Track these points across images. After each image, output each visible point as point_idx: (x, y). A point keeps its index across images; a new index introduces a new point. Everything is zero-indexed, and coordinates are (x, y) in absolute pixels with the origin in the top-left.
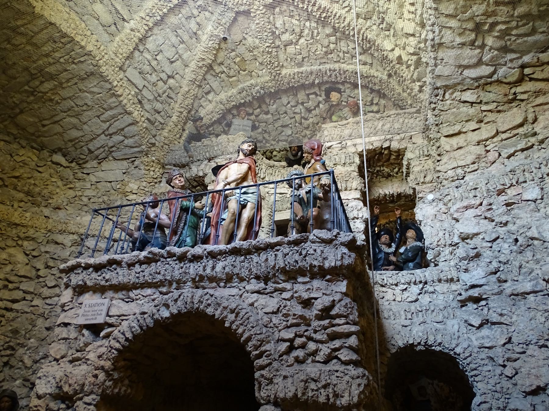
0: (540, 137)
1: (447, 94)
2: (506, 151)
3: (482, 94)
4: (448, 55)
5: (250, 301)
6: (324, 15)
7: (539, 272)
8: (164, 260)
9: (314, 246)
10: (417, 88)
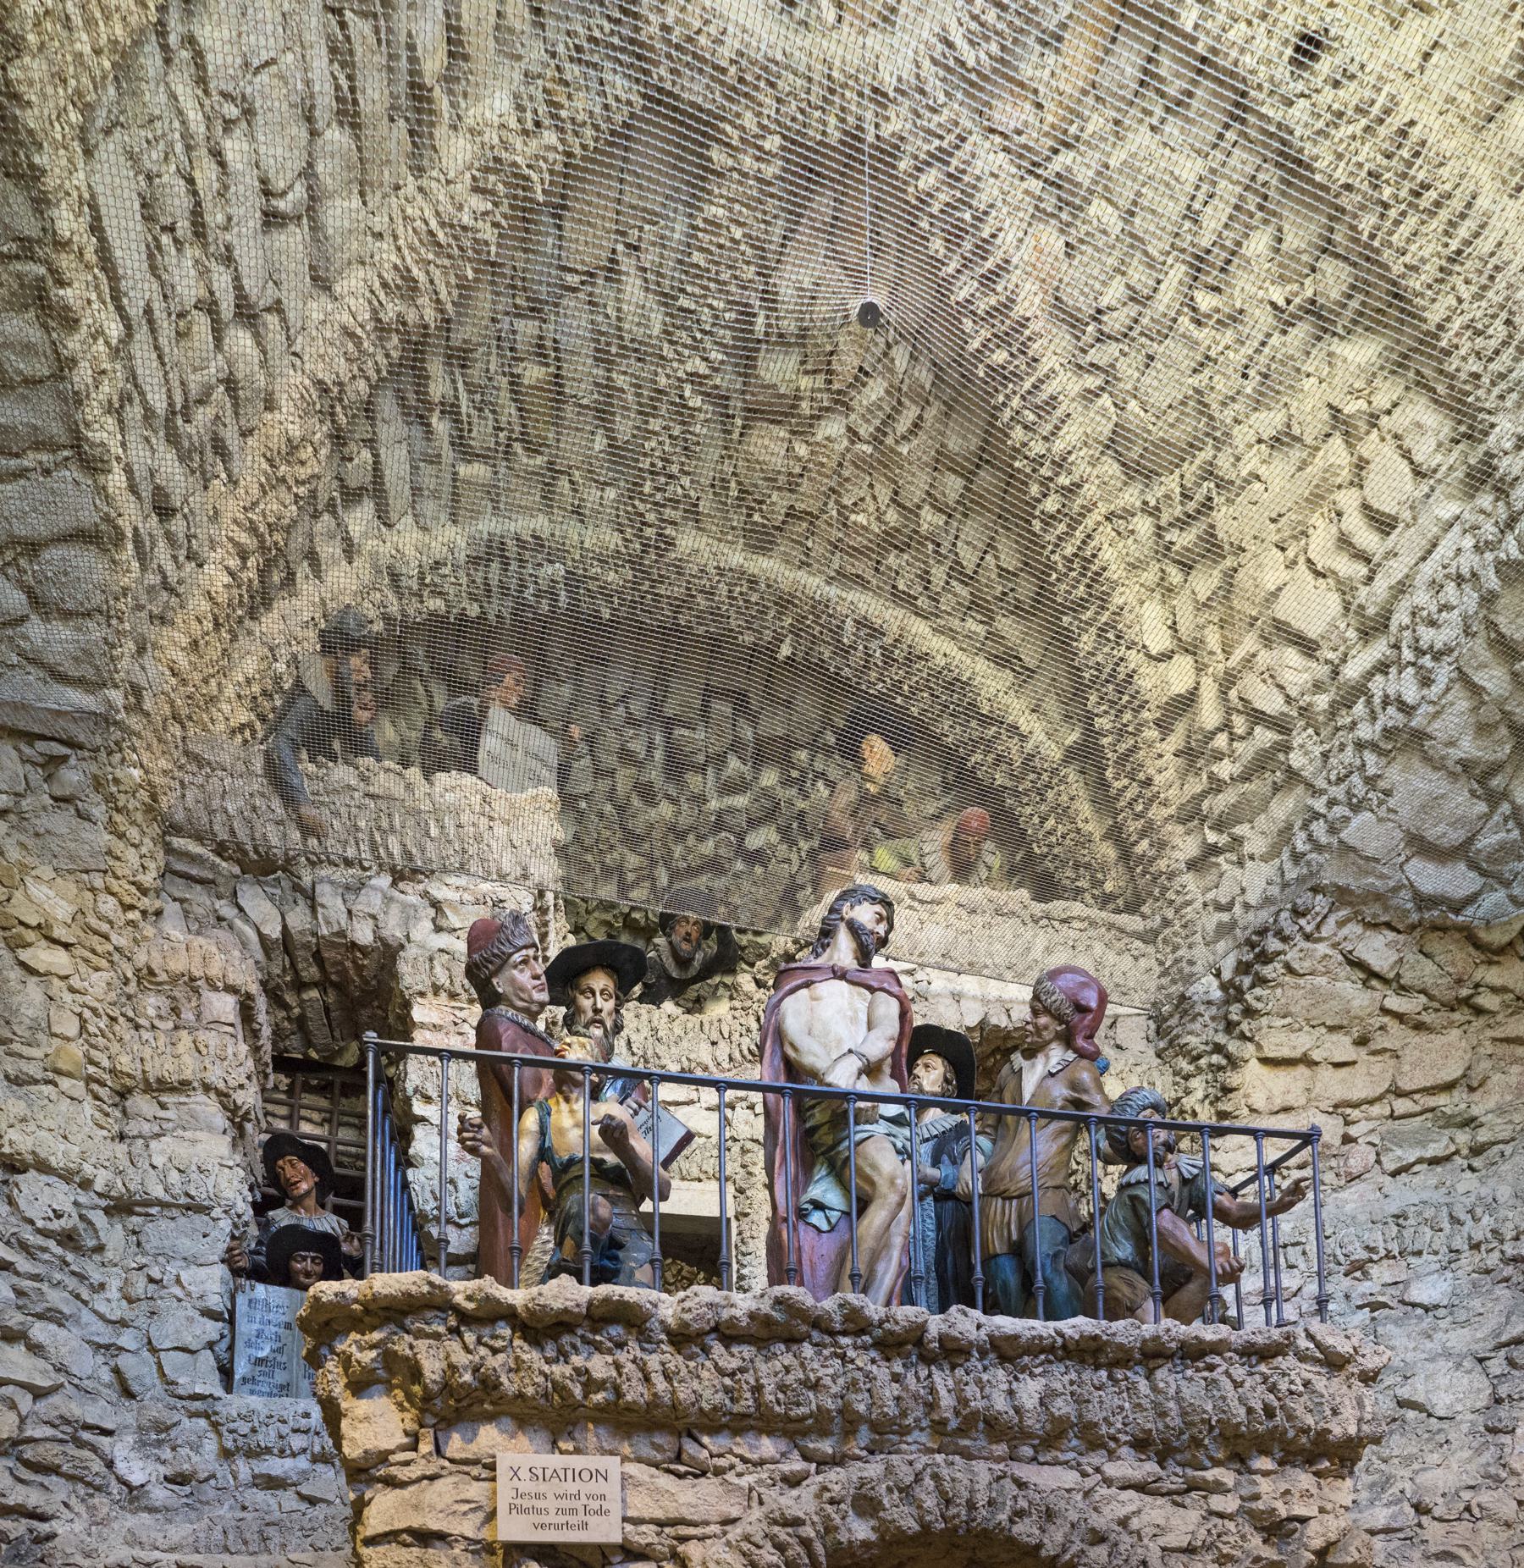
0: (1483, 1136)
1: (1332, 920)
2: (1399, 1152)
3: (1411, 957)
4: (1410, 782)
5: (1122, 1512)
6: (1000, 357)
7: (1408, 1486)
8: (828, 1339)
9: (1307, 1371)
10: (1186, 846)
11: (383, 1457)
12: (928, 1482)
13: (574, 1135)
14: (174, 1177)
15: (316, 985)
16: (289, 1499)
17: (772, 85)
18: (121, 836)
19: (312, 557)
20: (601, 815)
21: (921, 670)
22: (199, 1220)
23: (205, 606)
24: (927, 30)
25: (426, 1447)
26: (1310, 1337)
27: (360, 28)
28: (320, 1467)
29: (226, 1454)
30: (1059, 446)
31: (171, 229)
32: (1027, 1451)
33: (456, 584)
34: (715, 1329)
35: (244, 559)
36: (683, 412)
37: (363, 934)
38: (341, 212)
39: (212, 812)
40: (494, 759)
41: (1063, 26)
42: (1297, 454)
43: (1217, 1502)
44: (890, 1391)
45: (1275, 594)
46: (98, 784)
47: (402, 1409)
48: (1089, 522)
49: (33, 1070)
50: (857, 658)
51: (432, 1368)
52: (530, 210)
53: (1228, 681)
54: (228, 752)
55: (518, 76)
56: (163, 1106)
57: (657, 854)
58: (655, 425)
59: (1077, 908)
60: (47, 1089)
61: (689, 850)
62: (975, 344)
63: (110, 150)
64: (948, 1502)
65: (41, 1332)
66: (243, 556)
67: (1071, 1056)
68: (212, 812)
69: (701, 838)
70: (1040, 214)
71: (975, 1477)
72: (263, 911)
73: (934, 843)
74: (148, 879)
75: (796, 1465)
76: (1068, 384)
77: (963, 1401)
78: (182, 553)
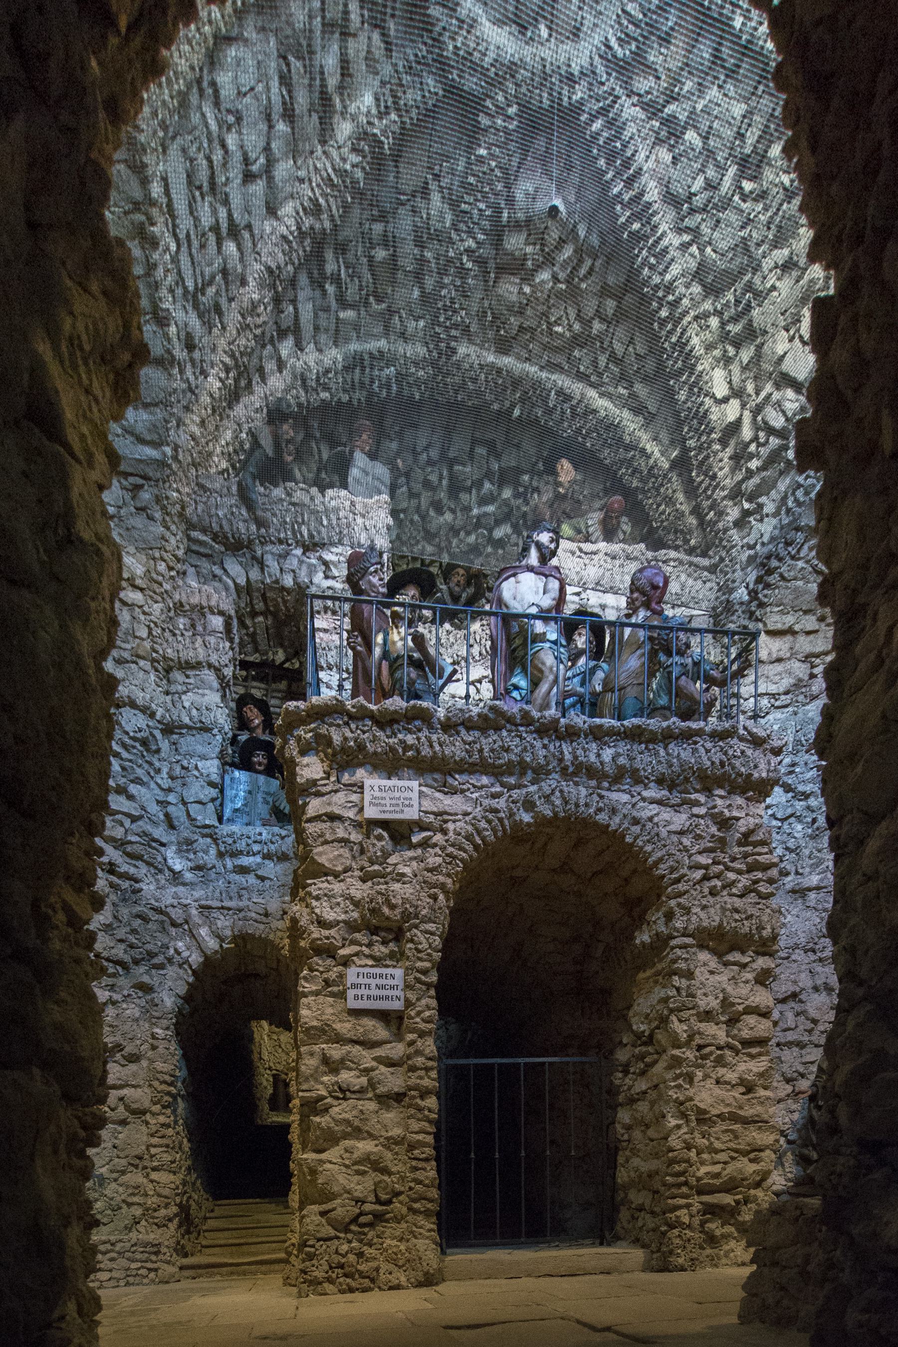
1: (806, 547)
5: (649, 814)
6: (636, 226)
9: (743, 746)
10: (734, 513)
11: (314, 782)
12: (557, 793)
13: (400, 644)
14: (194, 712)
15: (261, 614)
16: (251, 879)
17: (513, 76)
18: (168, 529)
19: (261, 370)
20: (412, 521)
21: (592, 421)
22: (206, 736)
23: (208, 400)
24: (597, 39)
25: (333, 779)
26: (745, 728)
27: (296, 64)
28: (267, 862)
29: (221, 855)
30: (668, 277)
31: (200, 188)
32: (606, 784)
33: (336, 381)
34: (463, 724)
35: (227, 372)
36: (462, 272)
37: (288, 581)
38: (283, 169)
39: (210, 516)
40: (358, 481)
41: (672, 29)
42: (795, 274)
43: (696, 810)
44: (542, 753)
45: (782, 358)
46: (158, 499)
47: (322, 761)
48: (685, 322)
49: (126, 655)
50: (557, 416)
51: (337, 738)
52: (380, 158)
53: (757, 411)
54: (218, 484)
55: (377, 83)
56: (188, 677)
57: (443, 544)
58: (446, 281)
59: (673, 554)
60: (133, 666)
61: (461, 541)
62: (623, 219)
63: (174, 149)
64: (566, 803)
65: (133, 789)
66: (227, 370)
67: (649, 614)
68: (210, 516)
69: (468, 533)
70: (659, 142)
71: (580, 792)
72: (235, 569)
73: (594, 519)
74: (180, 553)
75: (497, 789)
76: (673, 240)
77: (576, 757)
78: (198, 371)
